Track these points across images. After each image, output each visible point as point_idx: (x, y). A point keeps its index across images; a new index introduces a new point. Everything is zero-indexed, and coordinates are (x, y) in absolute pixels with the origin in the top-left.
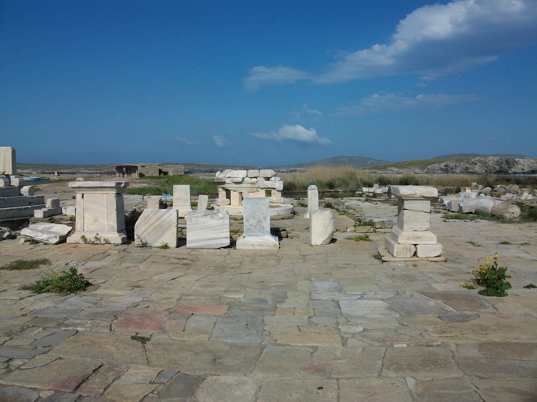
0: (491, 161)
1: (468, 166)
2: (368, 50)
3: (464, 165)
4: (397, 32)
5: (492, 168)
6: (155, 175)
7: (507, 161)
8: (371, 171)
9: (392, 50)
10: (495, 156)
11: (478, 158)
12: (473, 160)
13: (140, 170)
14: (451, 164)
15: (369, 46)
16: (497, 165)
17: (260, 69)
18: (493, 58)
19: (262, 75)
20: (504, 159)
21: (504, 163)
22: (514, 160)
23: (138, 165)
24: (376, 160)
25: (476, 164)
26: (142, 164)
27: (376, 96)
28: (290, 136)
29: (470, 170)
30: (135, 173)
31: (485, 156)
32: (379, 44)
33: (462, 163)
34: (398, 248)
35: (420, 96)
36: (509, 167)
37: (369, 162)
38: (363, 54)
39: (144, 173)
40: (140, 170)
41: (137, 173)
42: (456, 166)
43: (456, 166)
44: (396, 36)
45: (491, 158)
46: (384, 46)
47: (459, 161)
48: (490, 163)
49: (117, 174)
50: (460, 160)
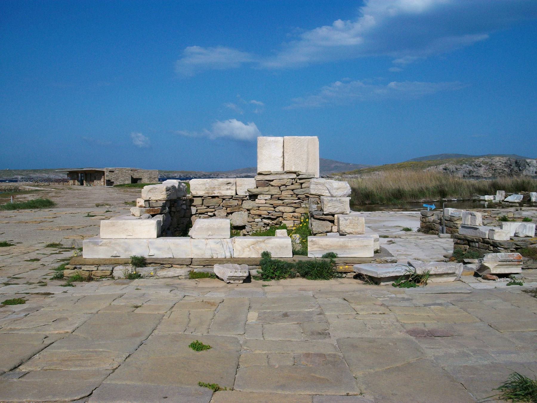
0: (498, 162)
1: (471, 168)
2: (329, 27)
3: (467, 168)
4: (364, 5)
5: (500, 171)
6: (127, 182)
7: (516, 162)
8: (353, 176)
9: (358, 27)
10: (502, 156)
11: (481, 159)
12: (477, 161)
13: (108, 176)
14: (452, 167)
15: (329, 22)
16: (506, 167)
17: (195, 49)
18: (484, 36)
19: (198, 57)
20: (513, 161)
21: (514, 165)
22: (525, 161)
23: (104, 170)
24: (341, 163)
25: (480, 166)
26: (110, 168)
27: (338, 83)
28: (226, 133)
29: (474, 174)
30: (100, 180)
31: (489, 156)
32: (342, 20)
33: (464, 165)
34: (495, 267)
35: (392, 84)
36: (520, 170)
37: (333, 166)
38: (323, 31)
39: (112, 181)
40: (108, 176)
41: (102, 180)
42: (457, 169)
43: (457, 169)
44: (364, 10)
45: (497, 159)
46: (348, 22)
47: (461, 163)
48: (498, 165)
49: (71, 182)
50: (461, 161)
